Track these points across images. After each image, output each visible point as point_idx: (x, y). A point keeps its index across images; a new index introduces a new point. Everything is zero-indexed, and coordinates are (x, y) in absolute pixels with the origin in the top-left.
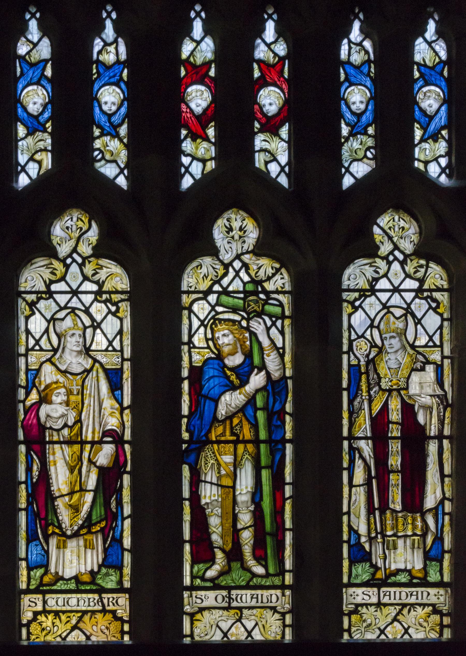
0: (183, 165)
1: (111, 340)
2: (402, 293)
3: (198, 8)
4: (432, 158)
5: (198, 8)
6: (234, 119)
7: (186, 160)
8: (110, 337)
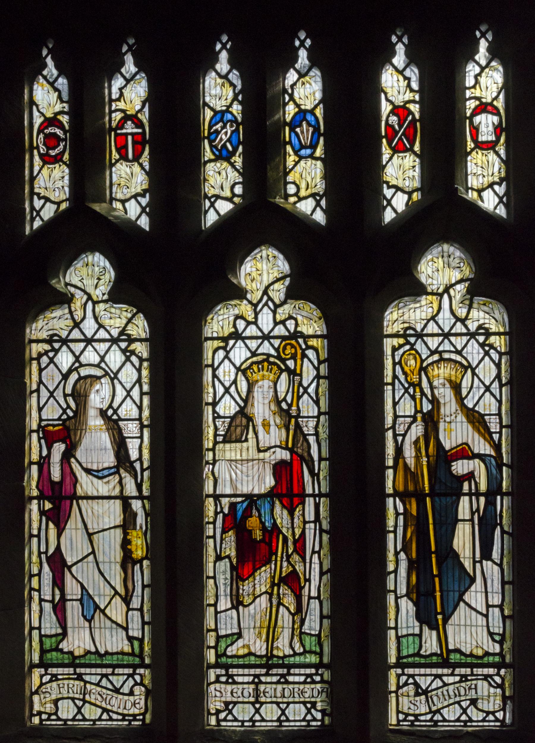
0: (385, 197)
1: (128, 398)
2: (83, 337)
3: (302, 35)
4: (484, 179)
5: (302, 35)
6: (262, 145)
7: (388, 193)
8: (227, 397)
